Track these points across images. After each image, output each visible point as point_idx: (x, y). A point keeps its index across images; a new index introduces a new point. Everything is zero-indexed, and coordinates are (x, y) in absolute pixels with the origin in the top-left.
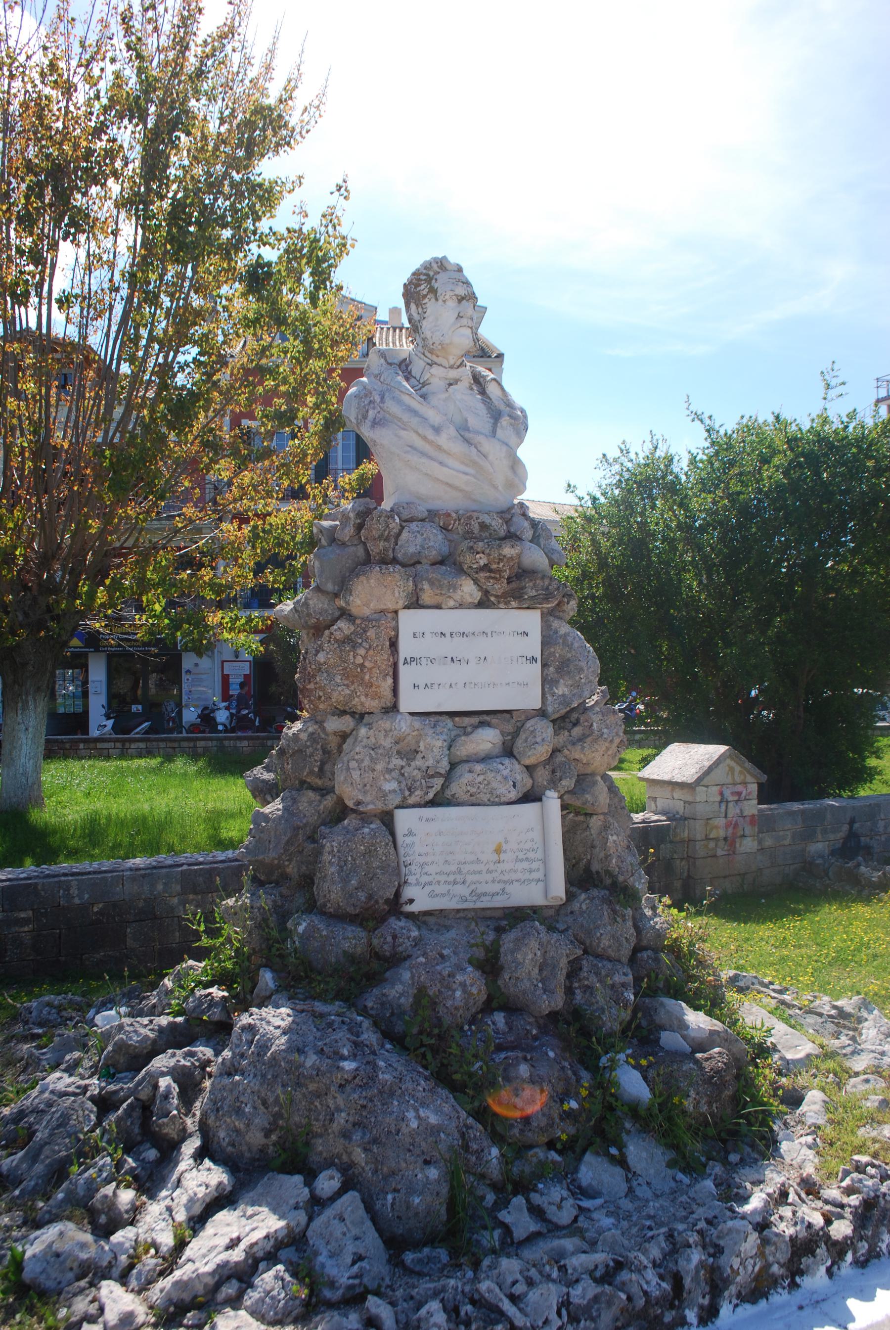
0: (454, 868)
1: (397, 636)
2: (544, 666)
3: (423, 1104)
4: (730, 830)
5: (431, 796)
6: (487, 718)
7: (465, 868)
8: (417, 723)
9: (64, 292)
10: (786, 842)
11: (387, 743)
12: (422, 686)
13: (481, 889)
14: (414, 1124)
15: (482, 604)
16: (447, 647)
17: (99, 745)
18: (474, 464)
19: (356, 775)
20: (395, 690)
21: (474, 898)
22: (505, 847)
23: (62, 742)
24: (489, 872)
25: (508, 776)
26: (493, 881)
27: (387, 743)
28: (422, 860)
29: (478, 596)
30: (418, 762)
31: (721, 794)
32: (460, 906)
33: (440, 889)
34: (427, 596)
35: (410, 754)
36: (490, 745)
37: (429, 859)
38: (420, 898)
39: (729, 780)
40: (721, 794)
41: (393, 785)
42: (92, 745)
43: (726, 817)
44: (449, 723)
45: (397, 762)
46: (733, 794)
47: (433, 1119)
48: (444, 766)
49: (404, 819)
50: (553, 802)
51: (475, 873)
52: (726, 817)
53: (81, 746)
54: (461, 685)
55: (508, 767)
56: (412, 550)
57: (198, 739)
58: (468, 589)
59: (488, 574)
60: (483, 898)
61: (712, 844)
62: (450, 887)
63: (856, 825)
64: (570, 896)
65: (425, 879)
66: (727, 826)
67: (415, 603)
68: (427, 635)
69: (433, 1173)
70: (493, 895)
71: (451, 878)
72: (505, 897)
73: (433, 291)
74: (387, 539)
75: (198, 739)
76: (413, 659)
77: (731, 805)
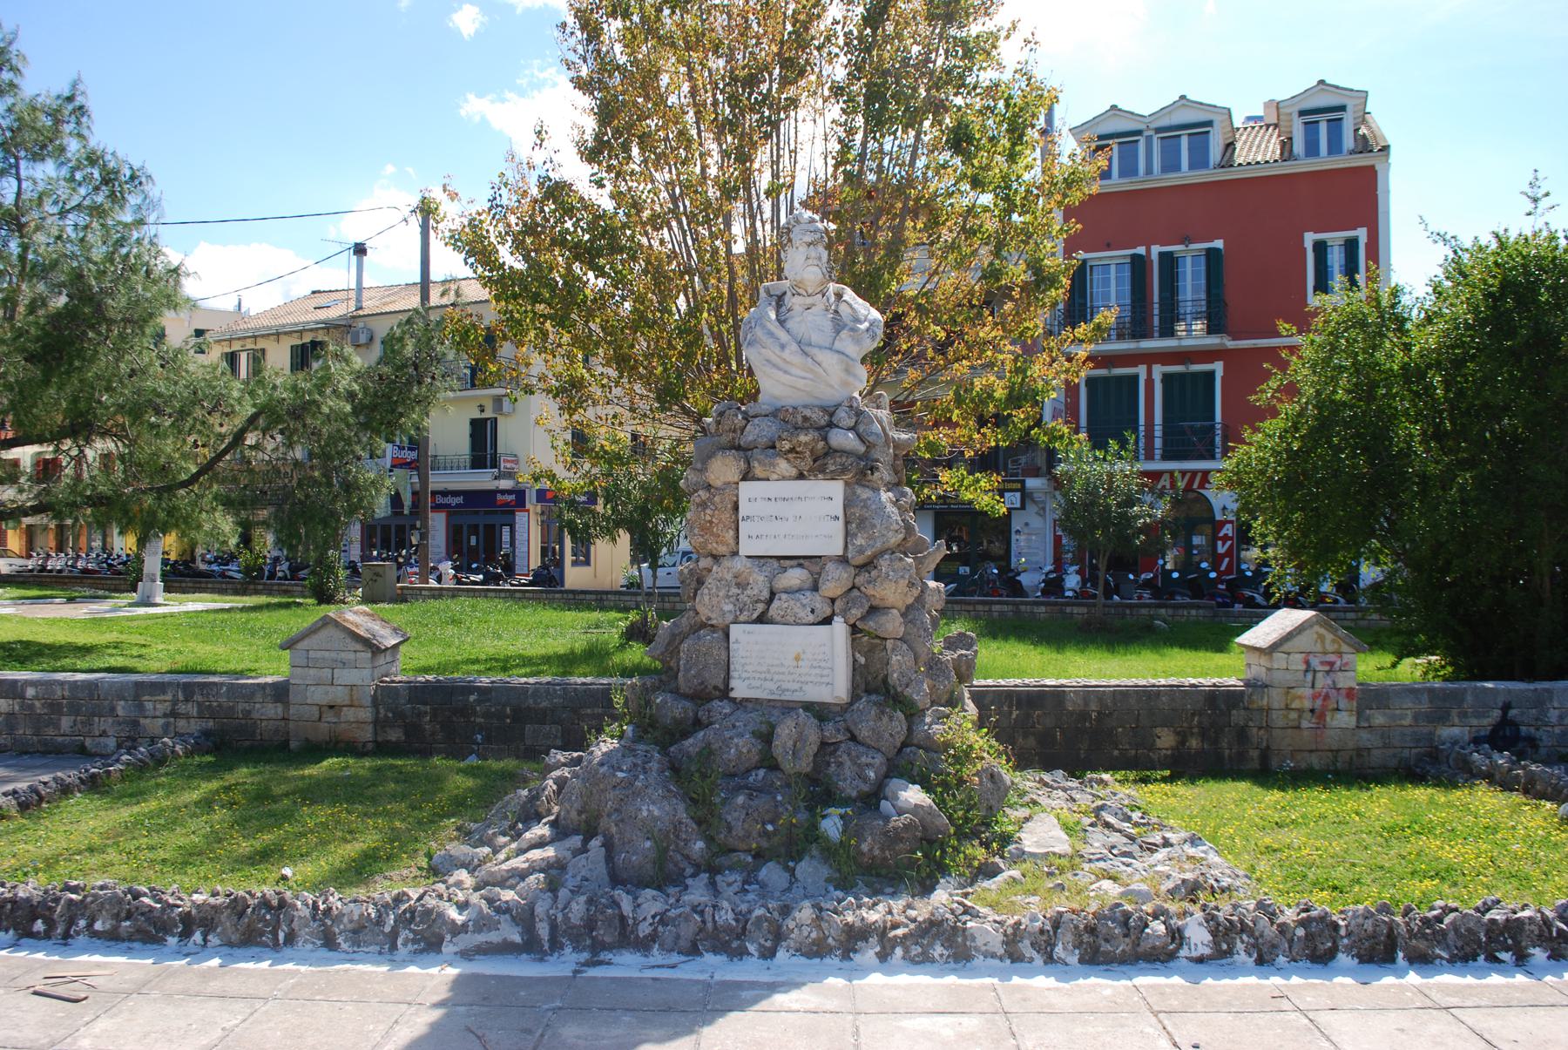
2: (847, 523)
3: (654, 803)
4: (1319, 702)
5: (755, 616)
7: (773, 670)
8: (749, 563)
10: (1405, 723)
11: (729, 577)
13: (785, 686)
14: (645, 814)
15: (801, 476)
16: (772, 509)
18: (811, 371)
19: (706, 598)
25: (801, 606)
27: (729, 577)
29: (794, 472)
30: (748, 592)
31: (1307, 663)
33: (758, 683)
34: (758, 470)
35: (742, 586)
38: (740, 690)
39: (1319, 648)
40: (1307, 663)
41: (730, 607)
43: (1313, 686)
44: (775, 564)
45: (734, 590)
46: (1322, 663)
47: (656, 813)
48: (766, 594)
49: (736, 631)
50: (839, 627)
52: (1313, 686)
55: (808, 598)
56: (750, 438)
57: (993, 603)
58: (783, 466)
61: (1293, 715)
63: (1513, 713)
64: (855, 697)
65: (744, 675)
66: (1315, 697)
67: (747, 476)
69: (648, 844)
73: (790, 240)
75: (993, 603)
77: (1319, 675)
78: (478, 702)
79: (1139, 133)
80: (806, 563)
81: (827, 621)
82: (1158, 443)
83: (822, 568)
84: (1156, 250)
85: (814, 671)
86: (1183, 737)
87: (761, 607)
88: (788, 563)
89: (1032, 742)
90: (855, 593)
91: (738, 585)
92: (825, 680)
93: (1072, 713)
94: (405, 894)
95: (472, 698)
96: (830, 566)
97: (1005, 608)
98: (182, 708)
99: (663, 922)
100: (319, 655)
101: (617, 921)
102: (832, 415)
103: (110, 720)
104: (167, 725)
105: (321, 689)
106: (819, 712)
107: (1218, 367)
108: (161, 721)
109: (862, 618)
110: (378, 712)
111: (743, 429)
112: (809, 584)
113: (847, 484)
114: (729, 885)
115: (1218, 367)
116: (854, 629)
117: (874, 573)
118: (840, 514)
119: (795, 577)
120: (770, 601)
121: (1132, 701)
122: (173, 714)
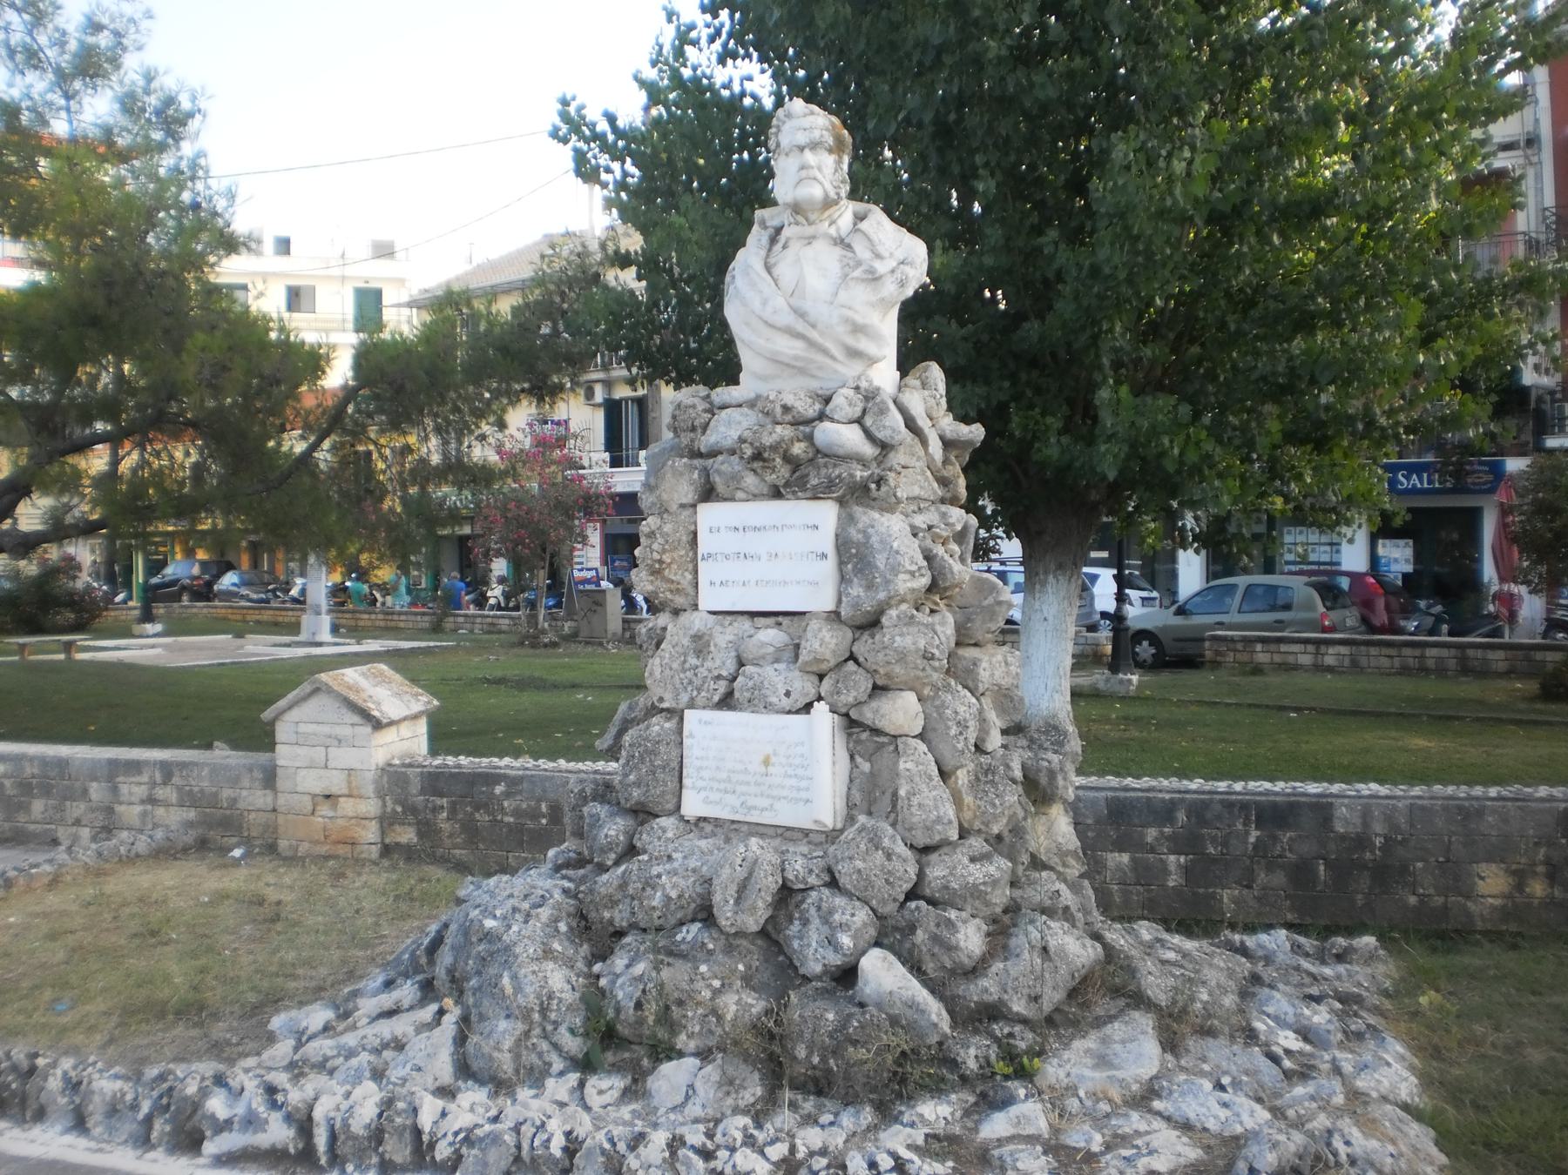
0: (724, 775)
2: (841, 564)
5: (716, 698)
13: (751, 801)
15: (776, 494)
16: (750, 543)
17: (1284, 648)
22: (773, 759)
23: (1232, 640)
24: (757, 784)
28: (698, 763)
30: (708, 664)
33: (715, 796)
42: (1273, 647)
53: (1259, 647)
54: (753, 582)
65: (700, 784)
71: (722, 786)
76: (710, 555)
78: (507, 795)
80: (785, 621)
86: (1520, 878)
87: (722, 687)
89: (1279, 879)
92: (803, 795)
93: (1343, 837)
94: (171, 1072)
95: (499, 789)
96: (814, 625)
97: (1445, 652)
98: (161, 793)
99: (468, 1141)
100: (311, 728)
101: (407, 1135)
102: (827, 400)
103: (83, 806)
104: (144, 814)
105: (313, 773)
108: (138, 809)
110: (384, 805)
111: (705, 427)
114: (601, 1092)
116: (851, 724)
122: (151, 800)
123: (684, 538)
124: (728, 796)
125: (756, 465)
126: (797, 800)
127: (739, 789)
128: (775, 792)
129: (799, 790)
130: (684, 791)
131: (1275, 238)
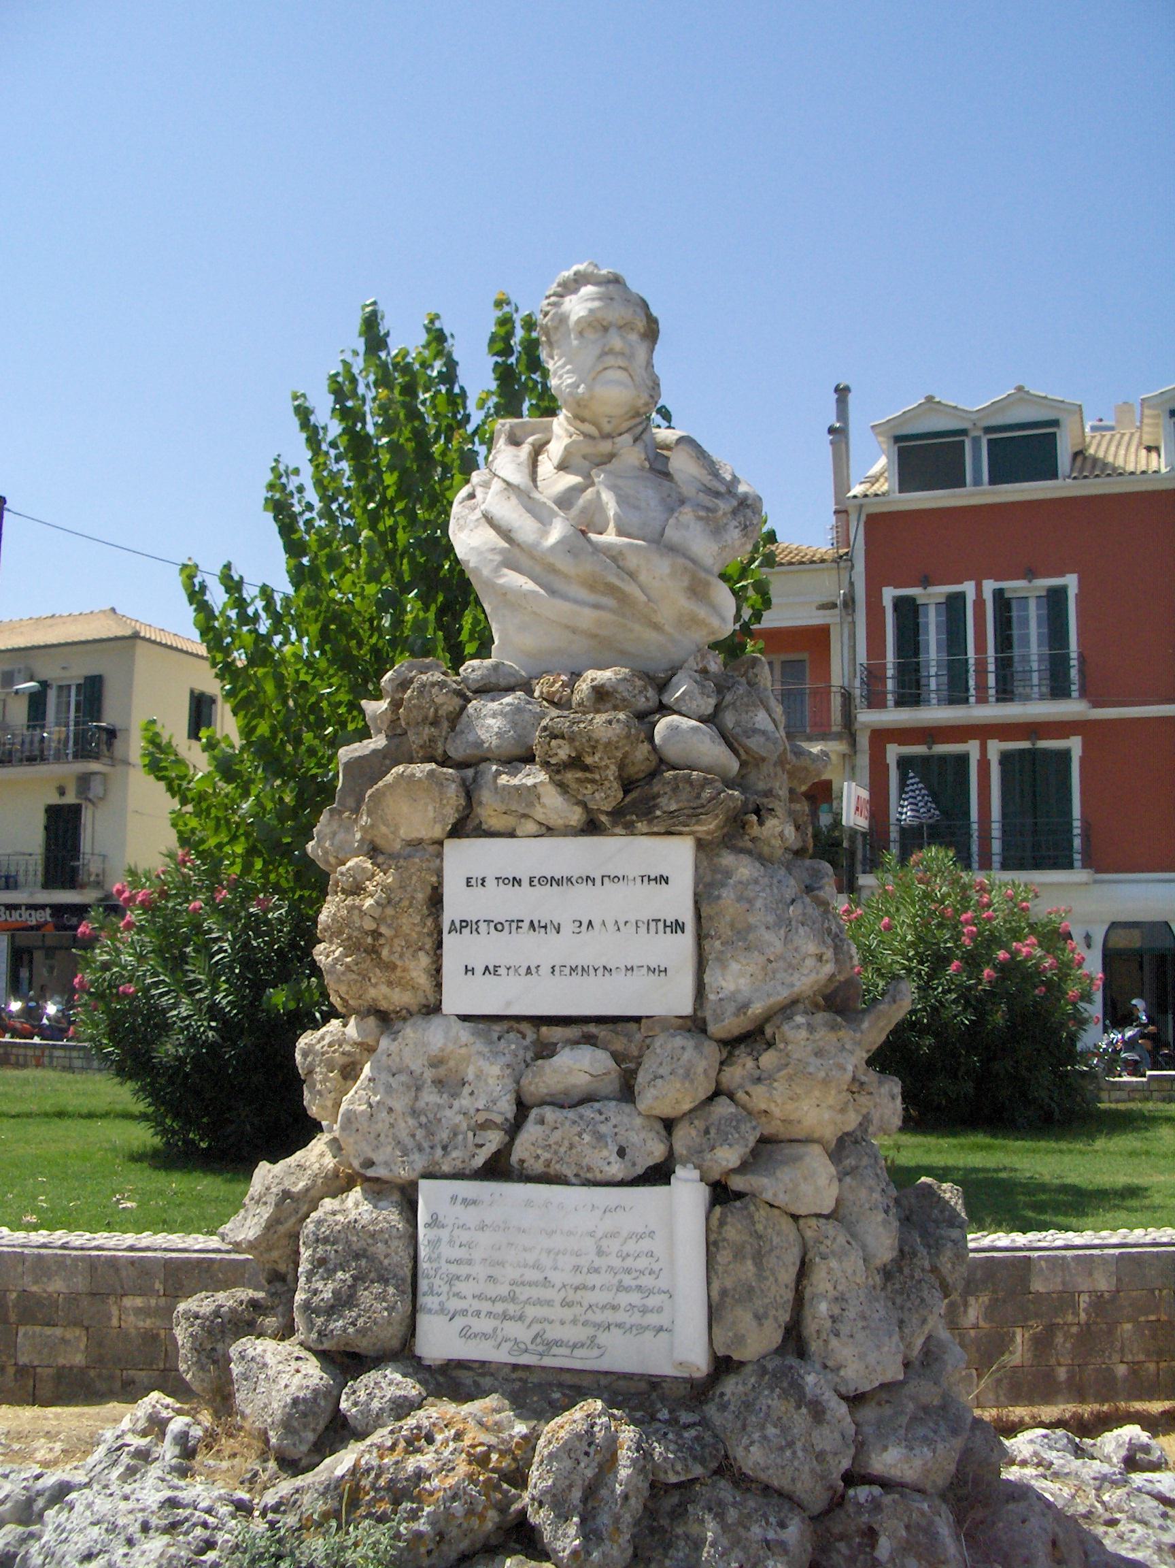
0: (503, 1290)
1: (441, 884)
5: (479, 1161)
6: (592, 1029)
7: (524, 1293)
8: (464, 1033)
9: (407, 354)
11: (417, 1065)
12: (479, 970)
13: (553, 1333)
15: (591, 827)
20: (436, 972)
21: (541, 1348)
24: (565, 1304)
26: (574, 1322)
28: (454, 1269)
29: (576, 816)
30: (465, 1101)
32: (513, 1360)
33: (485, 1325)
36: (588, 1077)
37: (463, 1270)
45: (430, 1097)
48: (506, 1107)
50: (687, 1194)
51: (539, 1302)
59: (579, 775)
60: (555, 1350)
62: (497, 1323)
65: (454, 1304)
68: (491, 882)
70: (574, 1346)
71: (499, 1308)
72: (596, 1352)
74: (435, 723)
76: (465, 924)
79: (963, 432)
81: (659, 1174)
82: (996, 846)
83: (645, 1046)
84: (989, 586)
85: (624, 1299)
87: (494, 1140)
88: (557, 1033)
90: (723, 1108)
91: (439, 1083)
92: (653, 1319)
102: (662, 686)
106: (636, 1395)
107: (1075, 745)
109: (744, 1168)
112: (611, 1084)
113: (700, 845)
115: (1075, 745)
116: (721, 1194)
117: (768, 1059)
118: (688, 918)
119: (578, 1066)
120: (514, 1127)
121: (988, 1220)
123: (420, 896)
124: (508, 1325)
125: (570, 776)
126: (642, 1329)
127: (531, 1312)
128: (599, 1317)
129: (644, 1311)
130: (418, 1316)
131: (446, 567)
